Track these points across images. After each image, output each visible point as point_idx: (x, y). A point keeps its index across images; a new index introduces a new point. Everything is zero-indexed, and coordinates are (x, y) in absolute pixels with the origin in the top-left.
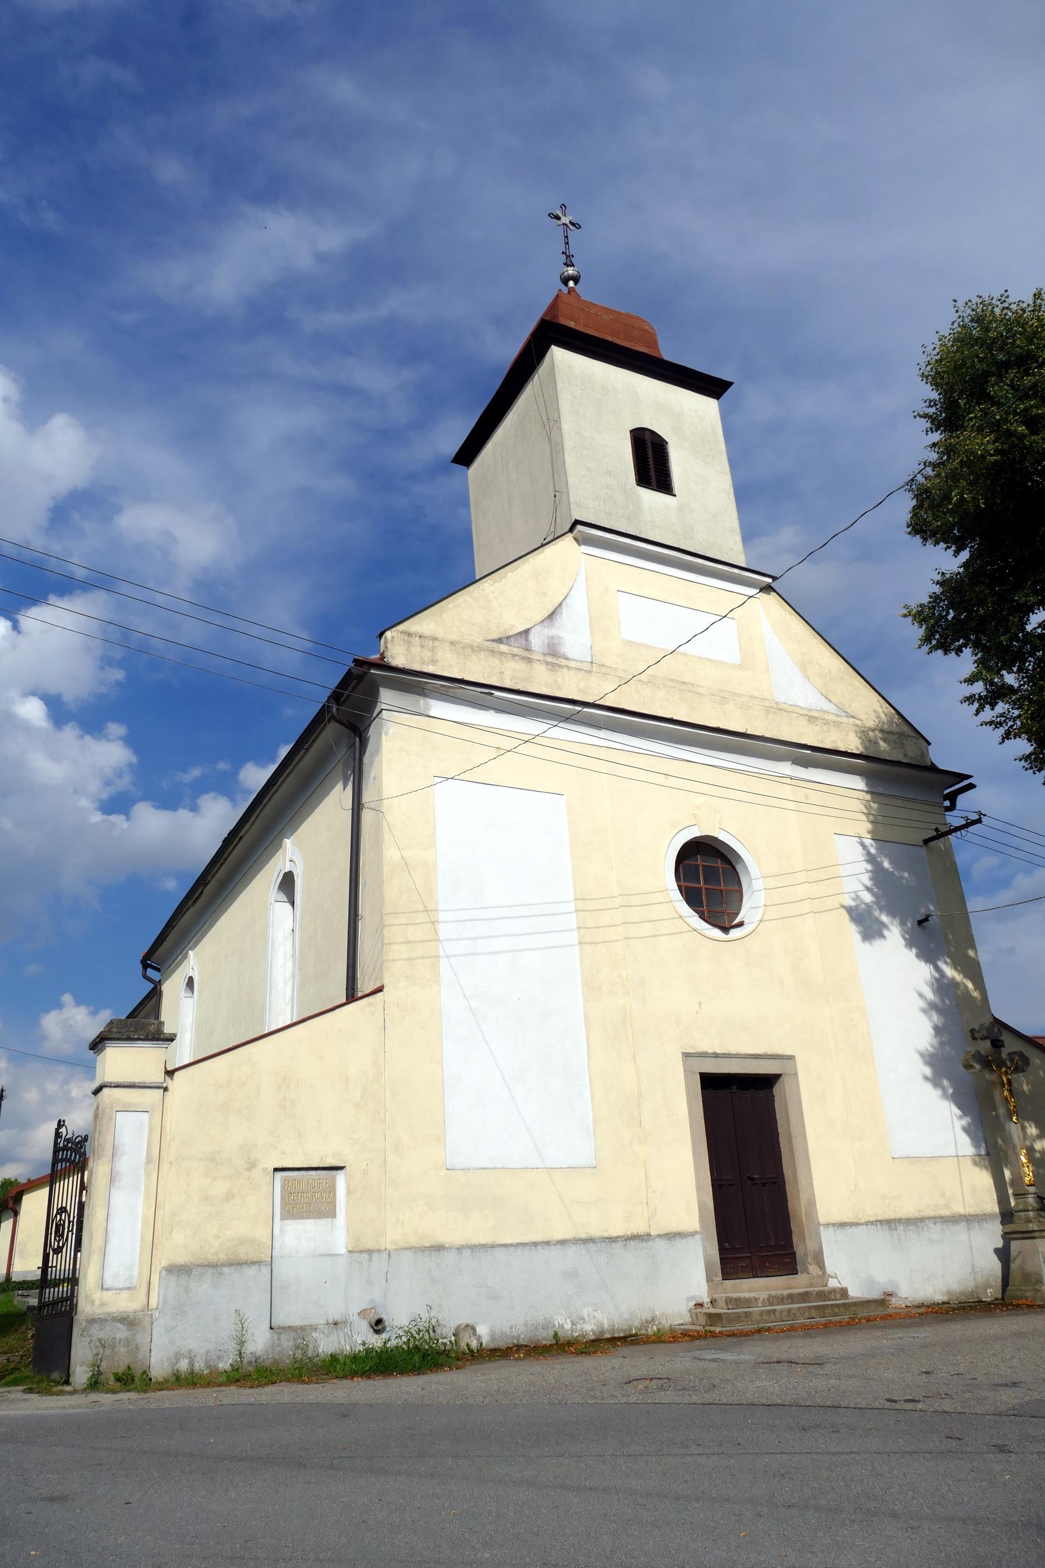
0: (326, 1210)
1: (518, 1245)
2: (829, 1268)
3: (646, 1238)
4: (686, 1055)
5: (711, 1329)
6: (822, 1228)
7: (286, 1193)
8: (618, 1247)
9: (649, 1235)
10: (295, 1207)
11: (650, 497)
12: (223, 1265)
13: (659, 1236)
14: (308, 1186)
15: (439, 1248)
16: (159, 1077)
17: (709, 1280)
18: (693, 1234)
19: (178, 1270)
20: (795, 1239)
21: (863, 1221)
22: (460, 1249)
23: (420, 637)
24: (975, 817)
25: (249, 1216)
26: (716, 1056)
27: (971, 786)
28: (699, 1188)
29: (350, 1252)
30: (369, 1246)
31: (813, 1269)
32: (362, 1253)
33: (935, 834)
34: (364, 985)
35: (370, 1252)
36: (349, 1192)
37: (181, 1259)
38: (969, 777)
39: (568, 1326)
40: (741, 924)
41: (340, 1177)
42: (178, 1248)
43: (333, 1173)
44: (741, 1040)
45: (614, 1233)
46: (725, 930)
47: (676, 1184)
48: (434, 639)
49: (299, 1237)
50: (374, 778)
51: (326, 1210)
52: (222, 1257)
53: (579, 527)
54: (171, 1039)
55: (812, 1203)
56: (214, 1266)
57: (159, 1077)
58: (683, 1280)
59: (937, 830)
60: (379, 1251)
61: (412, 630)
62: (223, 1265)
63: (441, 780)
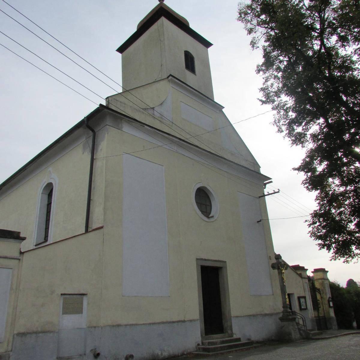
0: (79, 311)
1: (144, 324)
2: (234, 331)
3: (184, 321)
4: (197, 259)
5: (204, 350)
6: (232, 318)
7: (64, 303)
8: (175, 324)
9: (185, 320)
10: (67, 311)
11: (188, 73)
12: (40, 333)
13: (188, 321)
14: (73, 302)
15: (119, 326)
16: (17, 255)
17: (202, 336)
18: (198, 320)
19: (22, 335)
20: (223, 321)
21: (243, 316)
22: (126, 325)
23: (121, 102)
24: (277, 191)
25: (52, 313)
26: (205, 260)
27: (271, 182)
28: (199, 304)
29: (89, 327)
30: (95, 325)
31: (229, 332)
32: (92, 327)
33: (274, 192)
34: (94, 224)
35: (95, 327)
36: (88, 304)
37: (22, 331)
38: (270, 179)
39: (160, 354)
40: (212, 217)
41: (85, 298)
42: (21, 326)
43: (82, 296)
44: (212, 255)
45: (174, 320)
46: (208, 217)
47: (192, 305)
48: (125, 104)
49: (70, 321)
50: (101, 150)
51: (79, 311)
52: (39, 329)
53: (170, 77)
54: (24, 239)
55: (230, 310)
56: (36, 333)
57: (17, 255)
58: (192, 337)
59: (274, 191)
60: (98, 327)
61: (118, 99)
62: (40, 333)
63: (131, 154)
